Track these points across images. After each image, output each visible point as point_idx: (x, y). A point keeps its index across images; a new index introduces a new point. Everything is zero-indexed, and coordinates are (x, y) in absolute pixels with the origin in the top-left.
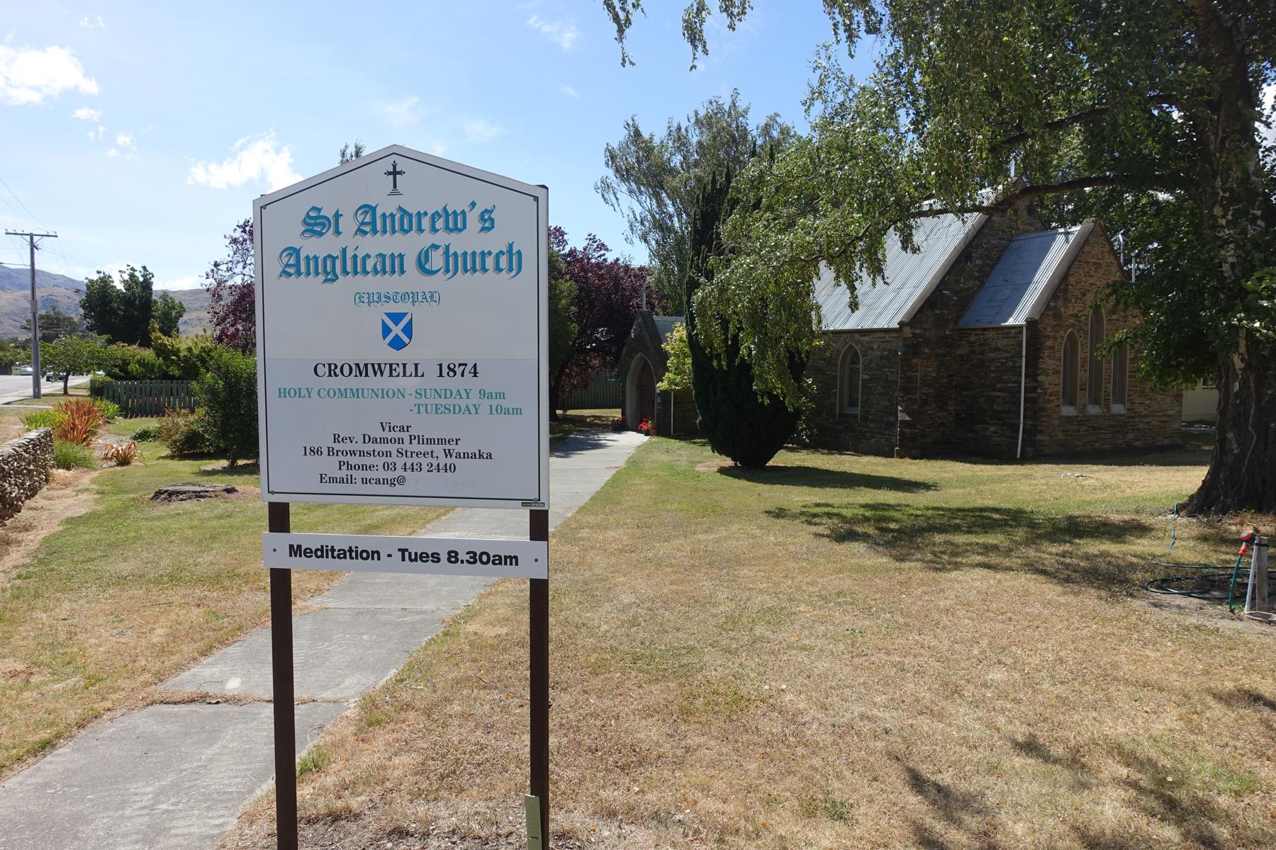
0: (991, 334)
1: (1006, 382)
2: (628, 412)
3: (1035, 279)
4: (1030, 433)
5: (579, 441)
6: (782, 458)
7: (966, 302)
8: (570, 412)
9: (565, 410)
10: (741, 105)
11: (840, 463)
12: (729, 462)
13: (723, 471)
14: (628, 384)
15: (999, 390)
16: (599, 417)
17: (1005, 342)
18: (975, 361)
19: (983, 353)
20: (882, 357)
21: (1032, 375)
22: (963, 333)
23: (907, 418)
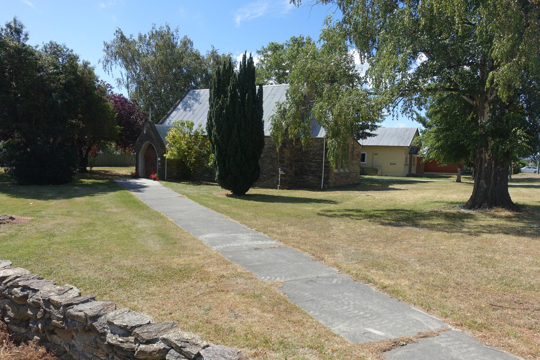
1: (316, 159)
4: (326, 179)
5: (122, 184)
6: (252, 191)
8: (95, 169)
9: (91, 166)
10: (172, 30)
12: (230, 192)
13: (228, 196)
14: (140, 156)
15: (314, 162)
16: (107, 171)
20: (269, 148)
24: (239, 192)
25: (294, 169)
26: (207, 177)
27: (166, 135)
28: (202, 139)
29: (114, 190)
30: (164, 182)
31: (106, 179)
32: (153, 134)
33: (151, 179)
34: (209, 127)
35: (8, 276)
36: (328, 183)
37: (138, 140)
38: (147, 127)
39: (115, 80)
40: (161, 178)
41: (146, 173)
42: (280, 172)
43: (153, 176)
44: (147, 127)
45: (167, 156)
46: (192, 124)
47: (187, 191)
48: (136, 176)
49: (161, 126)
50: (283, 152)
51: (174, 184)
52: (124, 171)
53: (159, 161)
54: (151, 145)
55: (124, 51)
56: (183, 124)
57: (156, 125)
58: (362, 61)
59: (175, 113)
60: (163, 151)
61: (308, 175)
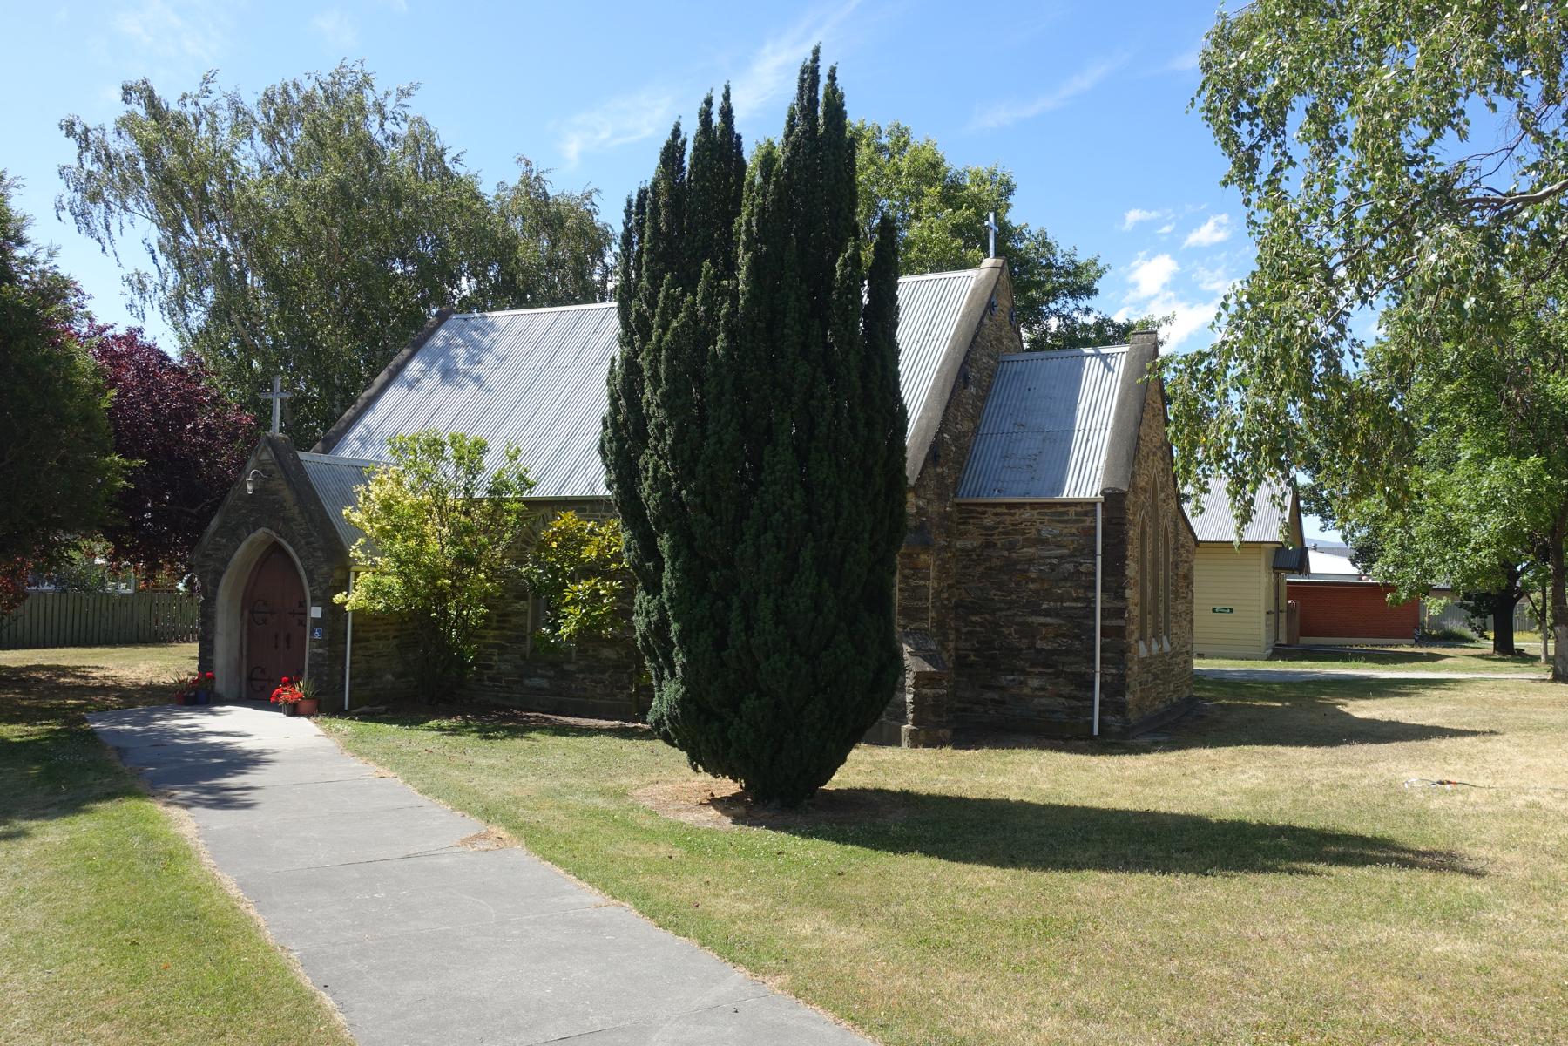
0: (1027, 514)
1: (1061, 599)
2: (220, 660)
3: (1079, 422)
4: (1114, 688)
6: (865, 768)
7: (962, 459)
11: (878, 765)
15: (1047, 613)
17: (1058, 528)
18: (996, 562)
19: (1011, 547)
21: (1115, 587)
22: (969, 512)
23: (929, 669)
24: (781, 779)
25: (951, 645)
26: (540, 690)
27: (351, 500)
28: (519, 513)
29: (71, 805)
30: (347, 726)
31: (49, 714)
32: (287, 495)
33: (275, 707)
34: (623, 441)
35: (676, 133)
36: (1121, 709)
37: (215, 523)
38: (260, 464)
39: (119, 284)
40: (324, 704)
41: (250, 679)
42: (909, 660)
43: (286, 695)
44: (260, 464)
45: (353, 599)
46: (481, 447)
47: (496, 788)
48: (198, 695)
49: (326, 458)
50: (915, 569)
51: (391, 734)
52: (143, 667)
53: (316, 622)
54: (276, 548)
55: (164, 164)
56: (435, 447)
57: (302, 455)
58: (1284, 154)
59: (393, 395)
60: (338, 574)
61: (1023, 672)
